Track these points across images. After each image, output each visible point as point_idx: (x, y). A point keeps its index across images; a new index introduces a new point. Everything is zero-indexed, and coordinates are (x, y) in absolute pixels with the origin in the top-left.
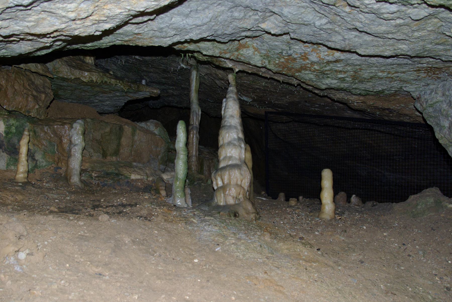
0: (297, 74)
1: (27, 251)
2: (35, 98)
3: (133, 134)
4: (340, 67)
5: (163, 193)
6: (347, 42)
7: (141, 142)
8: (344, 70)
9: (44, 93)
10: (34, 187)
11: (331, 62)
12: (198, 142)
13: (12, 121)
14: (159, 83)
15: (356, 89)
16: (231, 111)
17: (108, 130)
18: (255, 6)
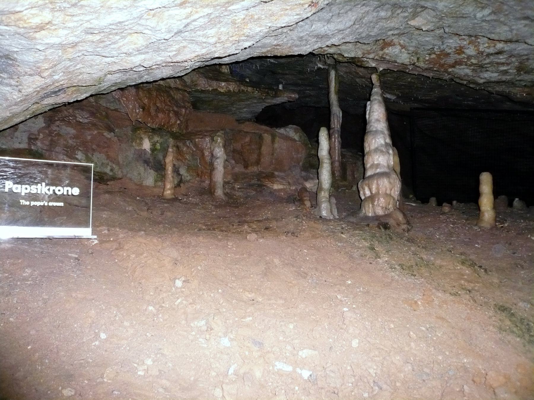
0: (450, 70)
1: (183, 279)
2: (177, 114)
3: (273, 141)
4: (502, 59)
5: (308, 204)
6: (515, 32)
7: (281, 149)
8: (507, 62)
9: (184, 107)
10: (181, 203)
11: (492, 54)
12: (340, 146)
13: (156, 138)
14: (296, 85)
15: (520, 80)
16: (376, 114)
17: (247, 139)
18: (404, 2)
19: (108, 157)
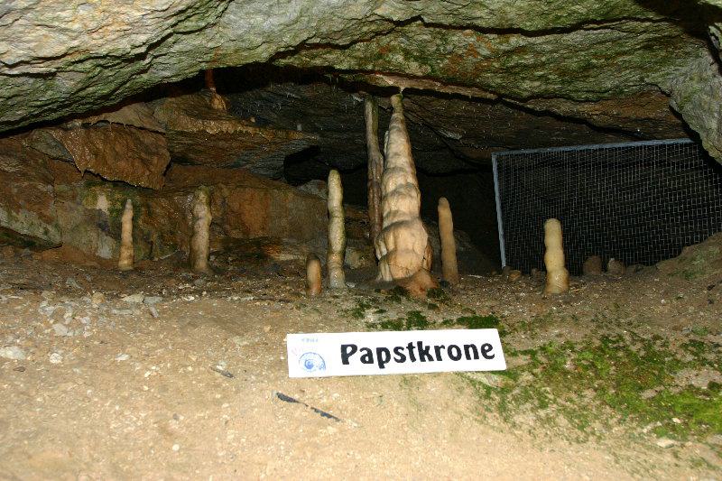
2: (145, 163)
9: (157, 154)
19: (41, 216)
